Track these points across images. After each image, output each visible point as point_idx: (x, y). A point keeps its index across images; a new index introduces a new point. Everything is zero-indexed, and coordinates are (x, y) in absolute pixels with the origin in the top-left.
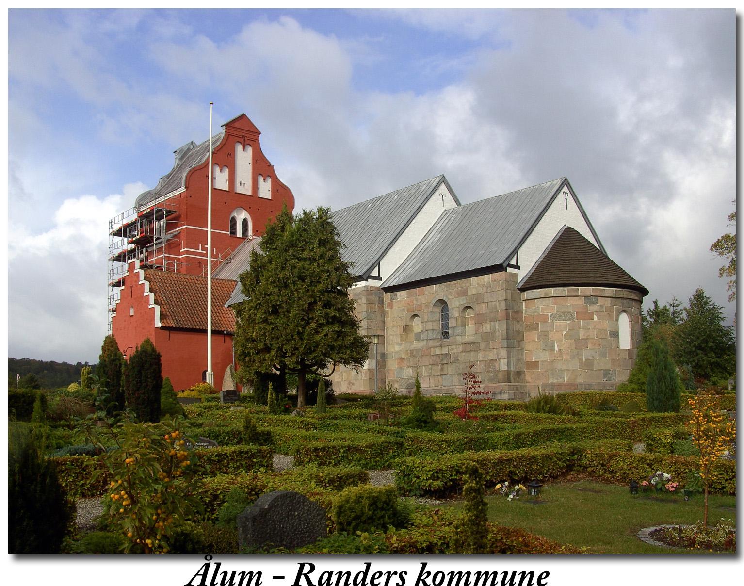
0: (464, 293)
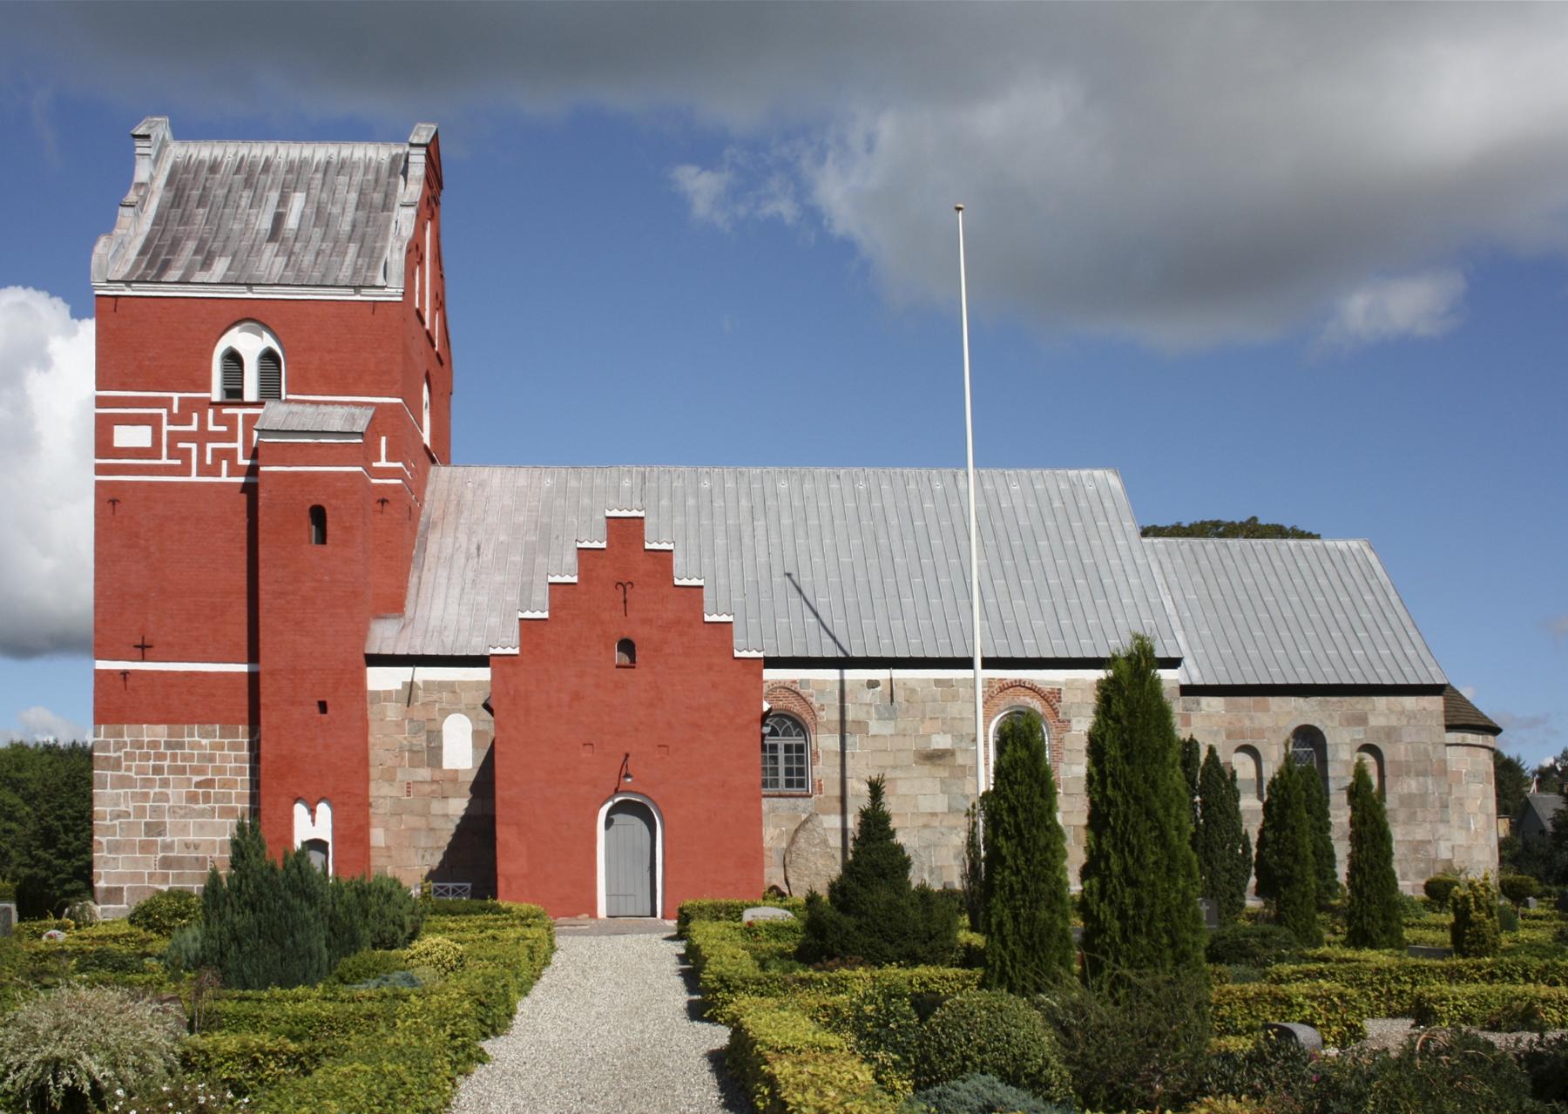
0: (1361, 720)
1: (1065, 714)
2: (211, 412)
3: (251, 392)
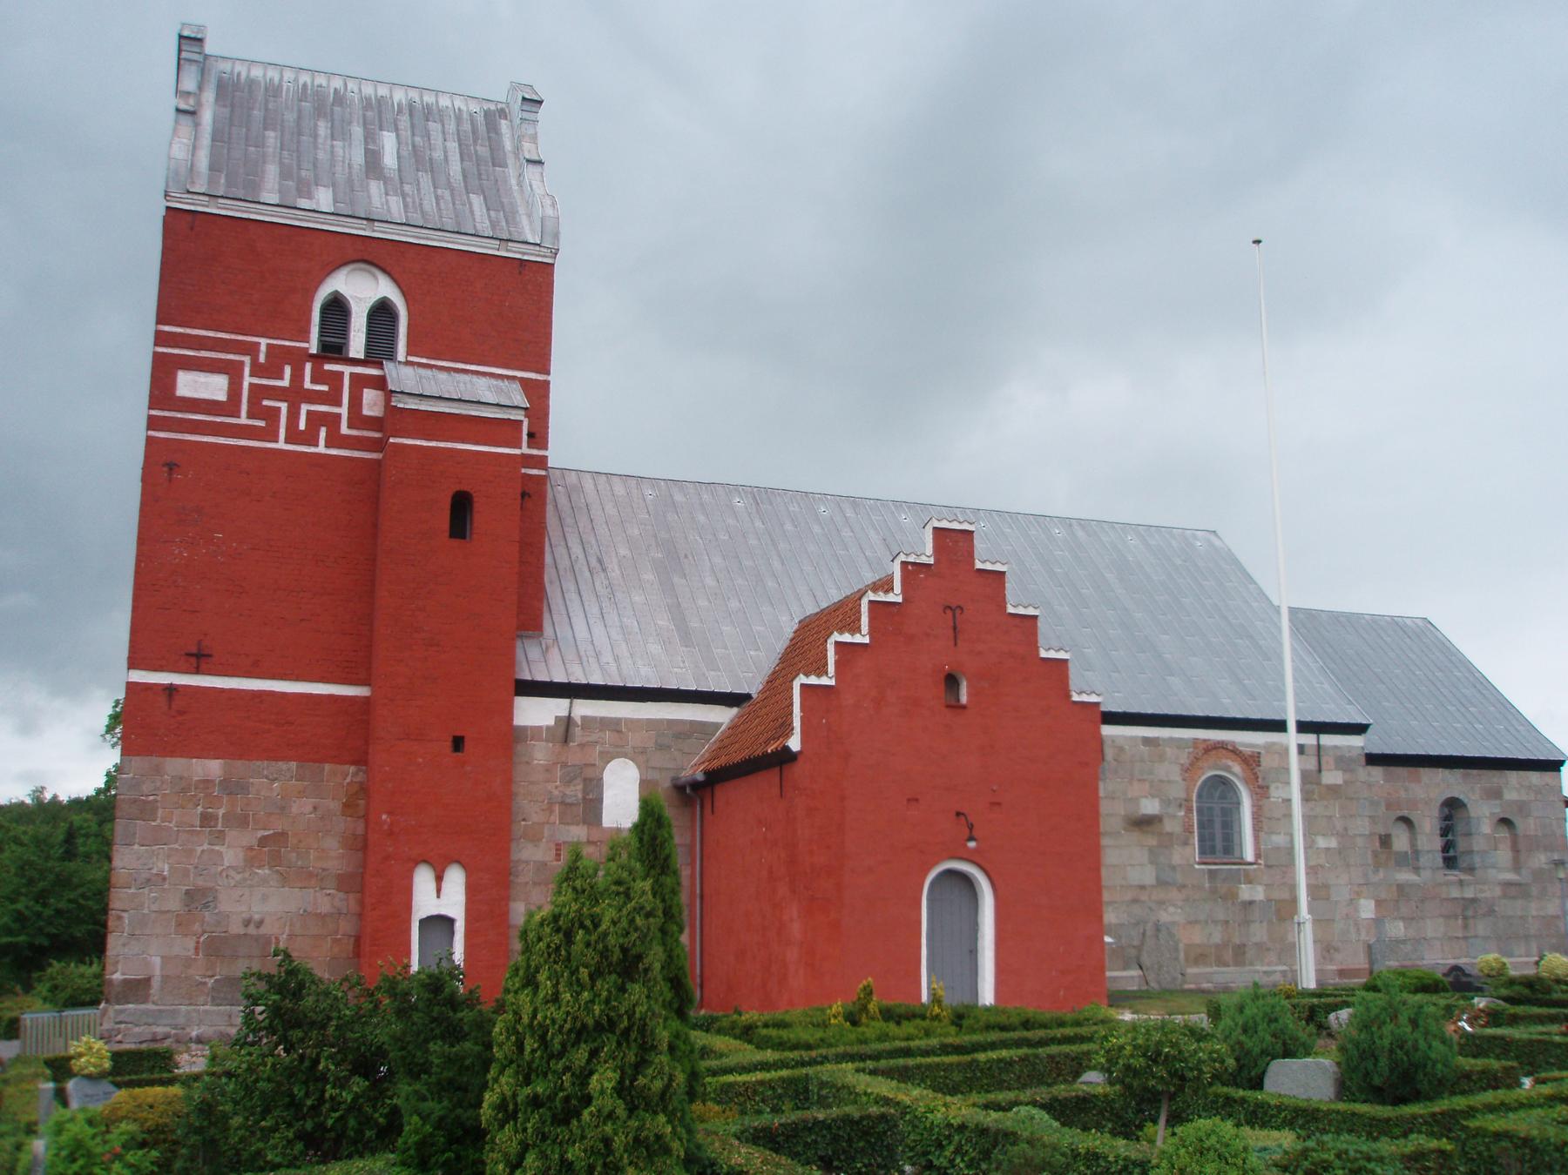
0: (1496, 794)
1: (1264, 779)
2: (308, 367)
3: (357, 344)
